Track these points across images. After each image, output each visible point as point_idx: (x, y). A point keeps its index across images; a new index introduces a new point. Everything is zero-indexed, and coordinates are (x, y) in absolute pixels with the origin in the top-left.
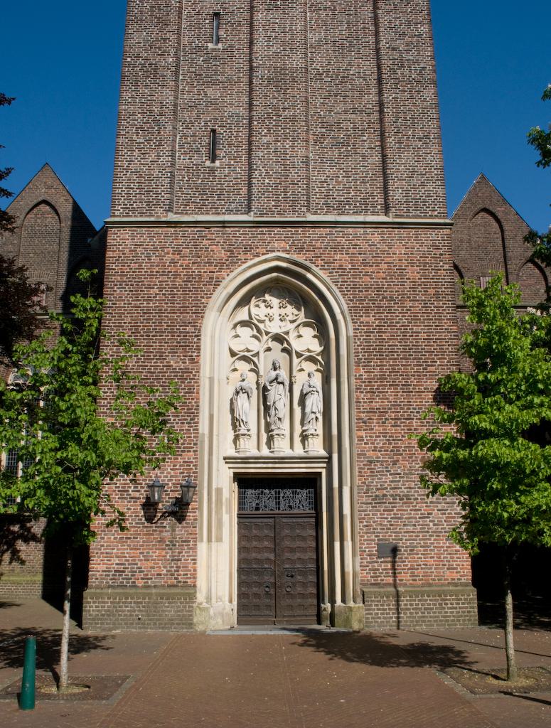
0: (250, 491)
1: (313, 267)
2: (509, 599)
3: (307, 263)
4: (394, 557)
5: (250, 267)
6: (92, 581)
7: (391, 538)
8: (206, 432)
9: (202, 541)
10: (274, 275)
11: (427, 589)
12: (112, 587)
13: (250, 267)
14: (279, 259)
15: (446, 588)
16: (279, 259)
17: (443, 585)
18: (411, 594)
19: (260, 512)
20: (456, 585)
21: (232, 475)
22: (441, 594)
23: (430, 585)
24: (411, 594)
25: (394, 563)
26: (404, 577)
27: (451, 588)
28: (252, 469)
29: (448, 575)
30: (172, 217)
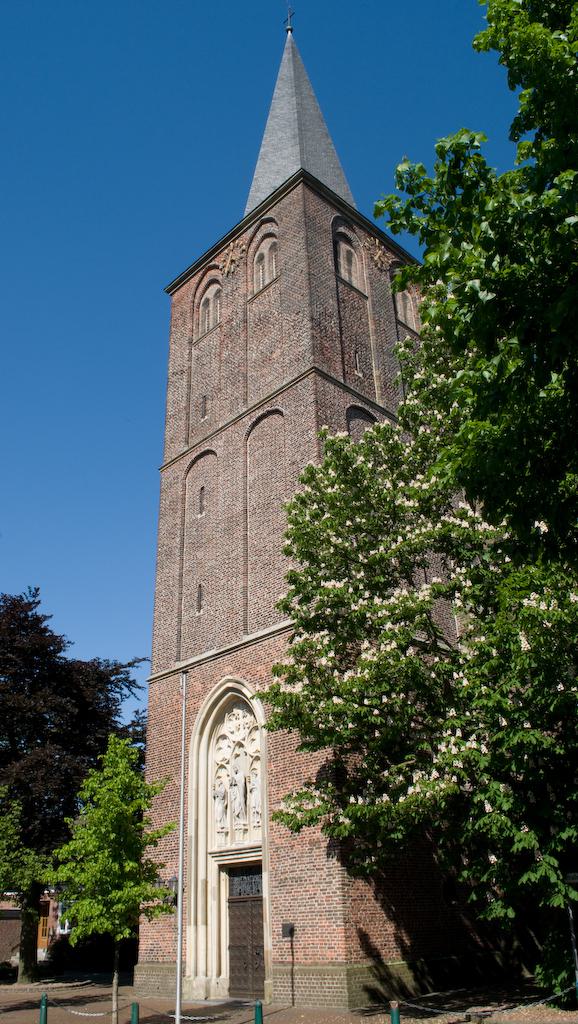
0: (236, 879)
1: (246, 683)
2: (500, 963)
3: (242, 680)
4: (292, 936)
5: (214, 692)
6: (141, 958)
7: (290, 920)
8: (193, 834)
9: (190, 924)
10: (230, 693)
11: (313, 968)
12: (148, 962)
13: (214, 692)
14: (229, 681)
15: (325, 968)
16: (229, 681)
17: (325, 964)
18: (304, 972)
19: (242, 896)
20: (333, 964)
21: (217, 867)
22: (321, 973)
23: (316, 964)
24: (304, 972)
25: (292, 941)
26: (299, 955)
27: (330, 967)
28: (228, 860)
29: (329, 954)
30: (247, 638)
